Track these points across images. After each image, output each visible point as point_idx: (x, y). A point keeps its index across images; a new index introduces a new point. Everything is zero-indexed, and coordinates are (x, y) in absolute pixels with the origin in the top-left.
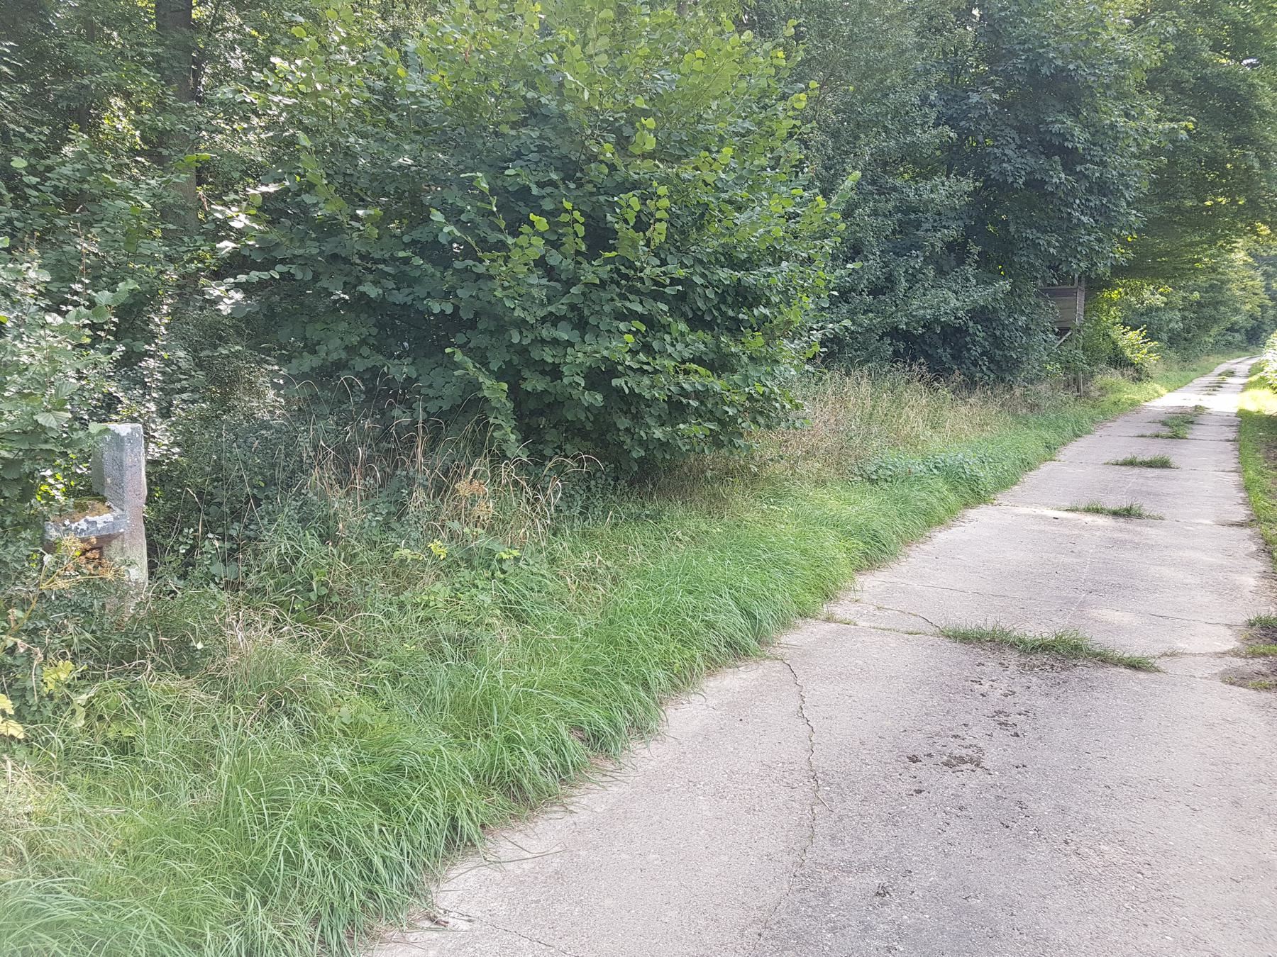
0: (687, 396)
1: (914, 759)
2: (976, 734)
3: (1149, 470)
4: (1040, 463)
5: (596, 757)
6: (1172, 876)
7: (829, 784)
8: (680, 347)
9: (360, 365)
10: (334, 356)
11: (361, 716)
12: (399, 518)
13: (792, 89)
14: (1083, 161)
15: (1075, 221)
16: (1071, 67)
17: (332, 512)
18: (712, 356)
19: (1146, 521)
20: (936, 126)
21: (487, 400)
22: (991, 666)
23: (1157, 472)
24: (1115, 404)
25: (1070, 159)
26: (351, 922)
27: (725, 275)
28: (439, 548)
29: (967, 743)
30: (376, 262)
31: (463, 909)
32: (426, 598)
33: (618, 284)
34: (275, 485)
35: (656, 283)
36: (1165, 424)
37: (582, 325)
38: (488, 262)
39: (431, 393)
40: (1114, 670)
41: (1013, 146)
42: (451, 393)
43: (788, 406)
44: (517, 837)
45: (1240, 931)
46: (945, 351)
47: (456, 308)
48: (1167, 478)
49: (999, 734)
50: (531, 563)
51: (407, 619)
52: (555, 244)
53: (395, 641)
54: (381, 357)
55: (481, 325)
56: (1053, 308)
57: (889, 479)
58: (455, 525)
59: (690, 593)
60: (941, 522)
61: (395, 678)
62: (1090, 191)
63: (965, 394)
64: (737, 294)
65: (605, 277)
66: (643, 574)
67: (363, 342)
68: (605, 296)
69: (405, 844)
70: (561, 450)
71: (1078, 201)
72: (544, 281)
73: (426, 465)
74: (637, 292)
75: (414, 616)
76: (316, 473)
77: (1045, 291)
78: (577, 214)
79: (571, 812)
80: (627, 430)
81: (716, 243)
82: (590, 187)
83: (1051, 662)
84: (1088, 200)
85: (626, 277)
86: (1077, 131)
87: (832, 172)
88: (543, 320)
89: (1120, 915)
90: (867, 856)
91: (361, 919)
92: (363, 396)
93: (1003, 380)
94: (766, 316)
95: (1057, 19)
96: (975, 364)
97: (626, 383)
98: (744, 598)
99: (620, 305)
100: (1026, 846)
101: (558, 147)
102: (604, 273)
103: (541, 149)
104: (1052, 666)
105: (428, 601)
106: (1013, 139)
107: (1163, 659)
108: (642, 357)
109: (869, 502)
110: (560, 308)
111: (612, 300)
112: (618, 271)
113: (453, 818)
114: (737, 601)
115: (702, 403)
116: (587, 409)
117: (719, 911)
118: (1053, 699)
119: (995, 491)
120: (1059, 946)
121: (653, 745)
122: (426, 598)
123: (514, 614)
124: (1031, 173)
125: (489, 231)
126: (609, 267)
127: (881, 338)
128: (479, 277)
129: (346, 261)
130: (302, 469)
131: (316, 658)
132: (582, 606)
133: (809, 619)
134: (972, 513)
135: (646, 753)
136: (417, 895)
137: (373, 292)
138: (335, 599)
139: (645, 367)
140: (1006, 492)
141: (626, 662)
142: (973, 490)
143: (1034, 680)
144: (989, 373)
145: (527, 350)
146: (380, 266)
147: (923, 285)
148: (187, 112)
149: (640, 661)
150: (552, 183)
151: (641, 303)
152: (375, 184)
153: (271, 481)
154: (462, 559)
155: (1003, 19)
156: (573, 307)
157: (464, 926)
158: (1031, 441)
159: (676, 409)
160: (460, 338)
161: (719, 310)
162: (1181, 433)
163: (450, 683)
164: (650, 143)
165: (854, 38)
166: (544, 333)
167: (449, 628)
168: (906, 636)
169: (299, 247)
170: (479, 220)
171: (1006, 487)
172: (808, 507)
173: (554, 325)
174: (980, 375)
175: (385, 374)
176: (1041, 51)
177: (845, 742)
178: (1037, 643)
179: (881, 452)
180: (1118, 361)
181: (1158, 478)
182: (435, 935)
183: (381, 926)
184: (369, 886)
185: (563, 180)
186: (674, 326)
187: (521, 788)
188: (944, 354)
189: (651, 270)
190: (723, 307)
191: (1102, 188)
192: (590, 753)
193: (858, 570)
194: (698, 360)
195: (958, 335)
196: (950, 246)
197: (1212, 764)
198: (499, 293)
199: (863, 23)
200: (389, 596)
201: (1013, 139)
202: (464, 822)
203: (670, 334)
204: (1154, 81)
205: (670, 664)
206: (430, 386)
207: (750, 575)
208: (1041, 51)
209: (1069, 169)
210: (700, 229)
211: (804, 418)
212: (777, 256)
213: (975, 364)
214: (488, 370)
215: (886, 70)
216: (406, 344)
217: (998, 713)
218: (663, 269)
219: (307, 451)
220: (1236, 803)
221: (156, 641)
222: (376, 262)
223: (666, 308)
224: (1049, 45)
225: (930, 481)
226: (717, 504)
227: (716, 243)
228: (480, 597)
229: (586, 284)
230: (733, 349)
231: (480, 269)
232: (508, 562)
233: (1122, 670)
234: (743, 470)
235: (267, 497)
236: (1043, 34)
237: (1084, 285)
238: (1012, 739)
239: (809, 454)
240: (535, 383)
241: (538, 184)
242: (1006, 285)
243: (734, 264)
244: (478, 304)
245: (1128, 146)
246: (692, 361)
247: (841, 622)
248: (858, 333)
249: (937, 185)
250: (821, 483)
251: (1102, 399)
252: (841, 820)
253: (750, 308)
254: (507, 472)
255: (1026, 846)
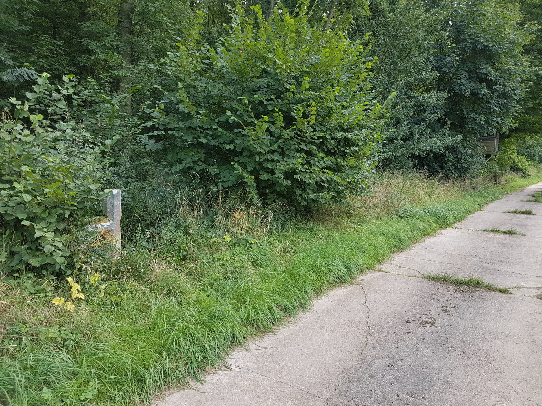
0: (323, 182)
1: (408, 322)
2: (433, 314)
3: (523, 215)
4: (475, 211)
5: (286, 317)
6: (503, 365)
7: (374, 329)
8: (321, 163)
9: (198, 168)
10: (189, 165)
11: (200, 298)
12: (212, 227)
13: (367, 60)
14: (496, 84)
15: (492, 110)
16: (490, 45)
17: (188, 224)
18: (334, 166)
19: (517, 236)
20: (432, 70)
21: (246, 182)
22: (443, 289)
23: (526, 216)
24: (512, 187)
25: (490, 84)
26: (198, 366)
27: (339, 135)
28: (228, 237)
29: (430, 317)
30: (205, 129)
31: (237, 364)
32: (223, 257)
33: (297, 138)
34: (166, 213)
35: (312, 138)
36: (533, 196)
37: (283, 154)
38: (247, 130)
39: (225, 179)
40: (493, 293)
41: (465, 79)
42: (232, 179)
43: (364, 187)
44: (256, 342)
45: (526, 384)
46: (436, 164)
47: (235, 147)
48: (529, 219)
49: (443, 314)
50: (262, 245)
51: (216, 265)
52: (273, 123)
53: (211, 272)
54: (206, 165)
55: (244, 154)
56: (483, 146)
57: (408, 217)
58: (234, 230)
59: (324, 258)
60: (429, 234)
61: (212, 285)
62: (499, 97)
63: (444, 182)
64: (345, 141)
65: (292, 136)
66: (306, 251)
67: (199, 160)
68: (292, 143)
69: (217, 341)
70: (274, 202)
71: (493, 101)
72: (269, 137)
73: (223, 207)
74: (304, 141)
75: (218, 263)
76: (181, 209)
77: (480, 139)
78: (280, 113)
79: (276, 335)
80: (300, 195)
81: (336, 122)
82: (286, 101)
83: (468, 289)
84: (498, 101)
85: (300, 136)
86: (493, 72)
87: (388, 90)
88: (268, 152)
89: (480, 377)
90: (386, 353)
91: (201, 365)
92: (199, 180)
93: (461, 176)
94: (356, 150)
95: (484, 25)
96: (449, 169)
97: (300, 177)
98: (345, 261)
99: (297, 146)
100: (448, 353)
101: (274, 85)
102: (292, 134)
103: (268, 86)
104: (468, 291)
105: (223, 258)
106: (465, 76)
107: (514, 289)
108: (306, 166)
109: (399, 225)
110: (275, 147)
111: (295, 144)
112: (297, 133)
113: (233, 334)
114: (342, 262)
115: (330, 185)
116: (285, 186)
117: (330, 369)
118: (466, 302)
119: (454, 222)
120: (455, 386)
121: (307, 313)
122: (223, 257)
123: (255, 264)
124: (473, 90)
125: (247, 117)
126: (293, 133)
127: (408, 158)
128: (243, 135)
129: (194, 129)
130: (176, 207)
131: (183, 277)
132: (282, 262)
133: (371, 270)
134: (443, 231)
135: (305, 316)
136: (221, 359)
137: (204, 141)
138: (189, 256)
139: (307, 171)
140: (459, 223)
141: (298, 283)
142: (444, 222)
143: (460, 295)
144: (455, 173)
145: (262, 163)
146: (207, 131)
147: (425, 137)
148: (131, 69)
149: (303, 282)
150: (272, 99)
151: (306, 145)
152: (205, 100)
153: (165, 212)
154: (236, 243)
155: (461, 26)
156: (280, 147)
157: (238, 370)
158: (471, 202)
159: (319, 187)
160: (236, 159)
161: (337, 148)
162: (539, 200)
163: (232, 288)
164: (308, 86)
165: (397, 36)
166: (269, 157)
167: (230, 268)
168: (410, 278)
169: (177, 124)
170: (244, 113)
171: (459, 221)
172: (373, 227)
173: (272, 154)
174: (451, 174)
175: (207, 172)
176: (477, 39)
177: (382, 315)
178: (462, 281)
179: (406, 206)
180: (515, 168)
181: (526, 218)
182: (227, 372)
183: (208, 368)
184: (204, 355)
185: (276, 98)
186: (319, 155)
187: (258, 325)
188: (436, 165)
189: (309, 133)
190: (339, 147)
191: (504, 96)
192: (284, 315)
193: (393, 252)
194: (329, 168)
195: (442, 157)
196: (439, 120)
197: (527, 328)
198: (251, 142)
199: (401, 29)
200: (209, 256)
201: (465, 76)
202: (237, 335)
203: (317, 157)
204: (527, 50)
205: (315, 284)
206: (224, 177)
207: (348, 252)
208: (477, 39)
209: (489, 87)
210: (329, 116)
211: (371, 192)
212: (361, 127)
213: (449, 169)
214: (247, 171)
215: (410, 48)
216: (215, 160)
217: (443, 307)
218: (314, 133)
219: (178, 201)
220: (534, 342)
221: (127, 268)
222: (205, 129)
223: (315, 148)
224: (481, 36)
225: (425, 218)
226: (336, 225)
227: (336, 122)
228: (243, 257)
229: (284, 139)
230: (342, 164)
231: (244, 133)
232: (254, 245)
233: (497, 293)
234: (347, 212)
235: (163, 218)
236: (478, 32)
237: (498, 136)
238: (448, 317)
239: (374, 206)
240: (264, 176)
241: (266, 100)
242: (460, 137)
243: (344, 130)
244: (243, 146)
245: (516, 77)
246: (325, 168)
247: (384, 272)
248: (398, 156)
249: (432, 96)
250: (379, 217)
251: (506, 185)
252: (377, 341)
253: (350, 147)
254: (253, 210)
255: (448, 353)
